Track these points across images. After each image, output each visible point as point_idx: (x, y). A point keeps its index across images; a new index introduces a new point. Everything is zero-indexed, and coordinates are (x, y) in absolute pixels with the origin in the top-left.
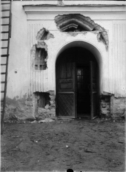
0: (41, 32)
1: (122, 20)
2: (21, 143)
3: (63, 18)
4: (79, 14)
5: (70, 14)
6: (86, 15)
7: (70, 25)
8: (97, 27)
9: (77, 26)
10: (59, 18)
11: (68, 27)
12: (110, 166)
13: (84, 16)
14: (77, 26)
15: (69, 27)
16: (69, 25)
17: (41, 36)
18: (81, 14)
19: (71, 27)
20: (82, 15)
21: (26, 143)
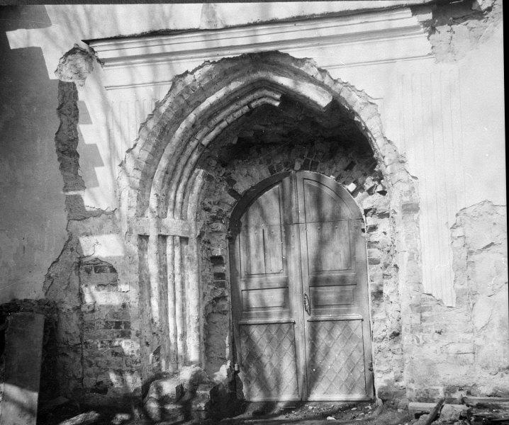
0: (151, 124)
1: (310, 29)
2: (76, 300)
3: (225, 73)
4: (276, 53)
5: (244, 57)
6: (296, 53)
7: (256, 94)
8: (341, 91)
9: (278, 96)
10: (208, 74)
11: (249, 104)
12: (64, 96)
13: (294, 59)
14: (278, 96)
15: (253, 105)
16: (249, 98)
17: (154, 140)
18: (281, 51)
19: (259, 102)
20: (286, 55)
21: (112, 384)
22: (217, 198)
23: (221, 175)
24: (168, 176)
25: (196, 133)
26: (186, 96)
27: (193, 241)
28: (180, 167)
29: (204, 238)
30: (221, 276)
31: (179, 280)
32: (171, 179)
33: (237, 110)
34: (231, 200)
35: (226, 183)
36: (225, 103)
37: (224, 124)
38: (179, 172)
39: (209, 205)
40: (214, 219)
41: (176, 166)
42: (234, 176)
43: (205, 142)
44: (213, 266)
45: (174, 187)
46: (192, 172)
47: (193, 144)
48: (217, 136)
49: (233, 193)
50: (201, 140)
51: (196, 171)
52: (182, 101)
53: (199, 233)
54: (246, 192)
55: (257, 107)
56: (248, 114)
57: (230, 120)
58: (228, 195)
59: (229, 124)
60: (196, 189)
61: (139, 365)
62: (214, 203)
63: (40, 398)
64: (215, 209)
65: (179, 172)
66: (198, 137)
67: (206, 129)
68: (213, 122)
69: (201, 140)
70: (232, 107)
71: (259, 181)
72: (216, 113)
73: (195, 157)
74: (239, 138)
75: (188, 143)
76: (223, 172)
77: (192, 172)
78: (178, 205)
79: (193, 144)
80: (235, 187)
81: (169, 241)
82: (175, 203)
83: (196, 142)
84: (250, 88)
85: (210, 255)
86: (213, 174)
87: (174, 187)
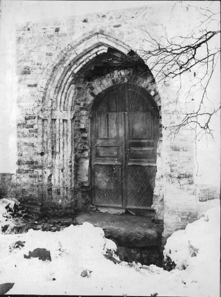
11: (96, 53)
15: (98, 53)
22: (84, 98)
23: (86, 85)
24: (57, 89)
25: (70, 68)
26: (65, 52)
27: (69, 122)
28: (63, 84)
29: (76, 119)
30: (85, 138)
31: (62, 141)
32: (59, 91)
33: (90, 56)
34: (91, 98)
35: (89, 89)
36: (85, 53)
37: (84, 63)
38: (63, 87)
39: (79, 102)
40: (82, 109)
41: (61, 84)
42: (93, 85)
43: (75, 72)
44: (81, 133)
45: (60, 94)
46: (69, 86)
47: (69, 73)
48: (81, 69)
49: (92, 94)
50: (74, 70)
51: (71, 86)
52: (63, 54)
53: (72, 117)
54: (100, 94)
55: (101, 54)
56: (96, 57)
57: (87, 61)
58: (90, 96)
59: (94, 58)
60: (71, 95)
61: (41, 182)
62: (82, 100)
63: (150, 95)
64: (82, 104)
65: (63, 87)
66: (72, 69)
67: (75, 66)
68: (79, 62)
69: (74, 70)
70: (88, 55)
71: (106, 87)
72: (81, 58)
73: (71, 79)
74: (95, 67)
75: (67, 72)
76: (88, 84)
77: (69, 86)
78: (63, 103)
79: (69, 73)
80: (93, 92)
81: (57, 121)
82: (61, 103)
83: (71, 72)
84: (97, 45)
85: (79, 128)
86: (81, 86)
87: (60, 94)
